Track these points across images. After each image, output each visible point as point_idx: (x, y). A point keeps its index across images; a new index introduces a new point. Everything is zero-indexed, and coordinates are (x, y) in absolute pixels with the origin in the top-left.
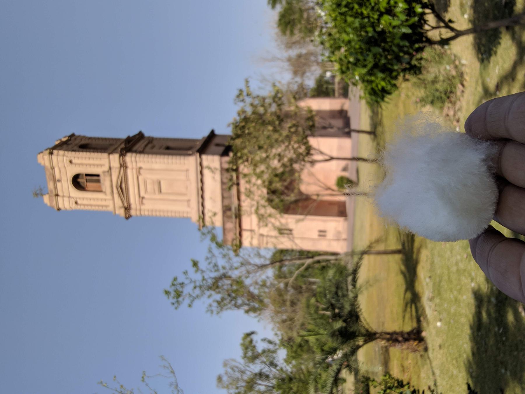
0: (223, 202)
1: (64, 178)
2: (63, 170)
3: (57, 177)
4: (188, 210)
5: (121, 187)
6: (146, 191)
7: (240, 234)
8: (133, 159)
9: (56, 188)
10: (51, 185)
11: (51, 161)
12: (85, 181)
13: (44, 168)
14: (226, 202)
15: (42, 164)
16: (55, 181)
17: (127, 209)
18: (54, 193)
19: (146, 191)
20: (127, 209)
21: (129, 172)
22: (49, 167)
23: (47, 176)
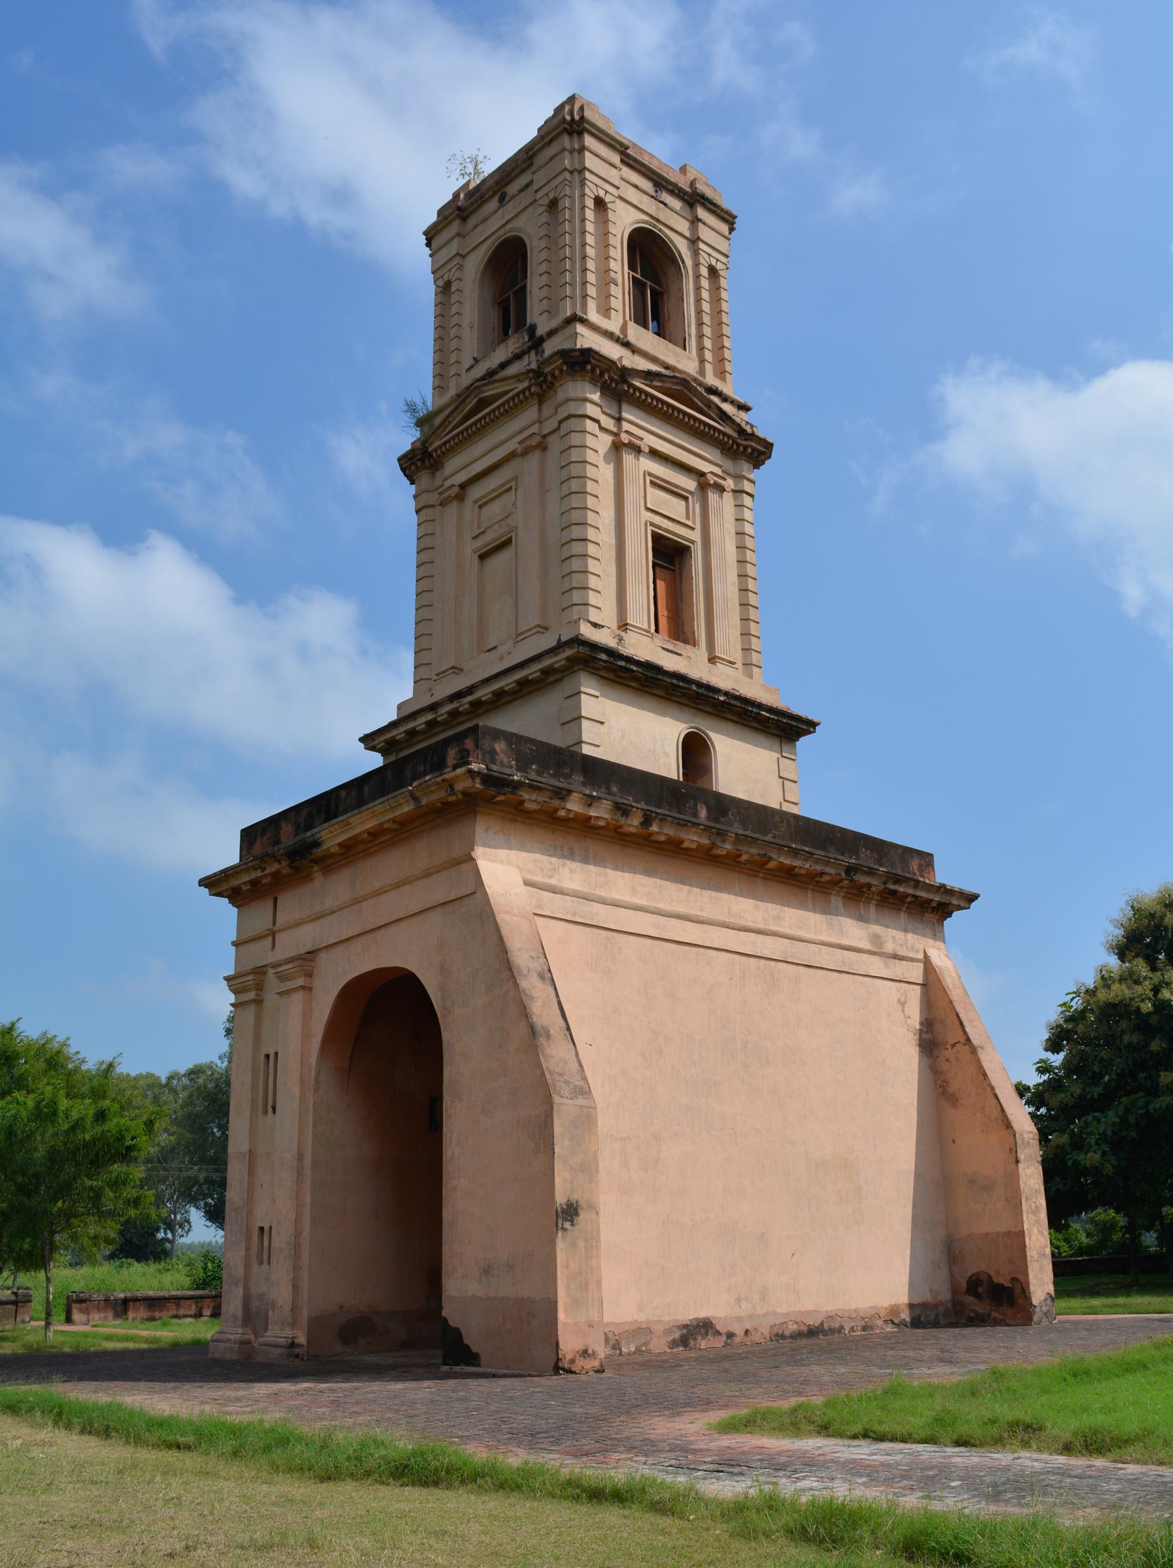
21: (530, 414)
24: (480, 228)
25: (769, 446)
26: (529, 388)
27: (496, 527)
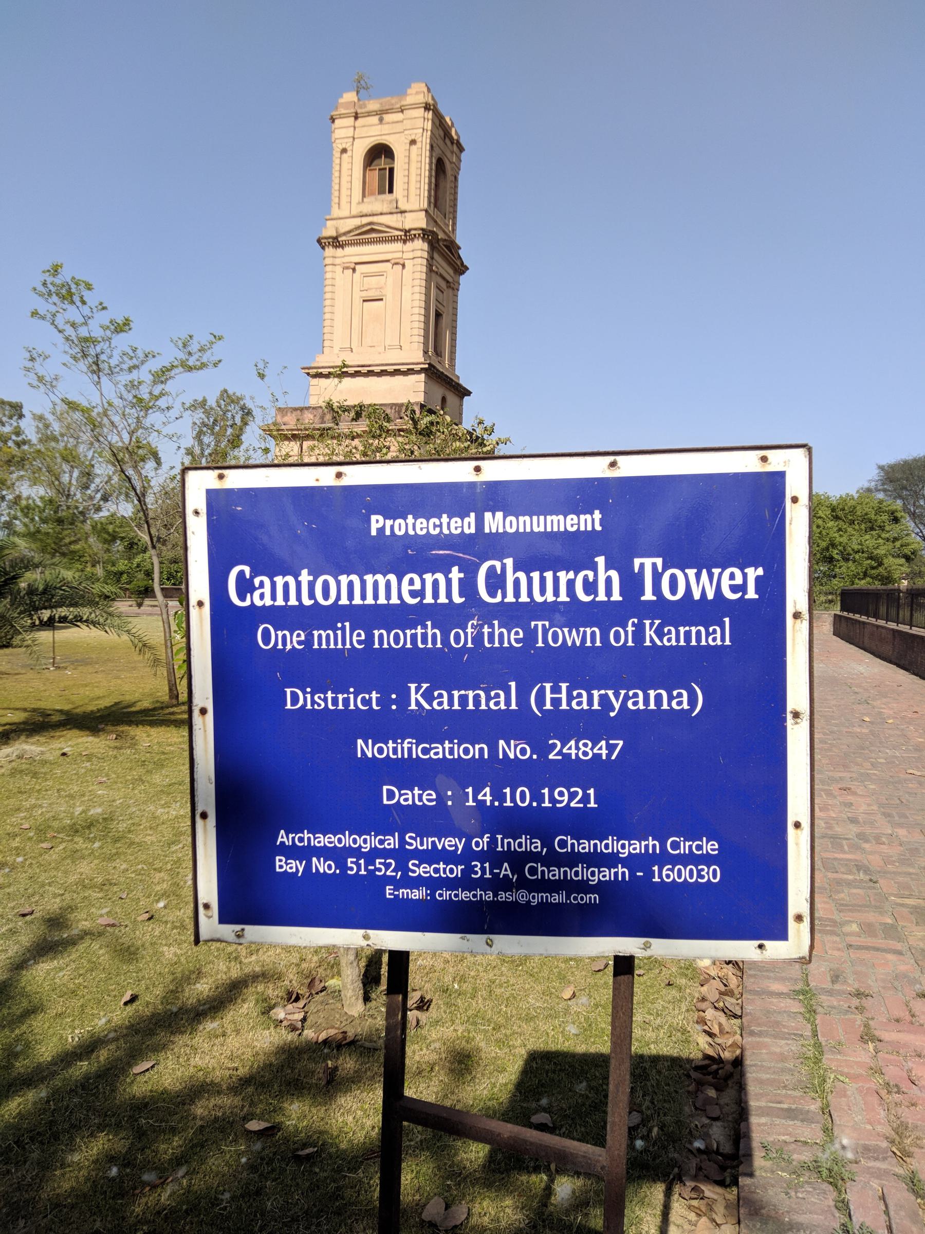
1: (386, 129)
2: (399, 127)
3: (388, 118)
4: (336, 350)
5: (372, 230)
6: (366, 276)
7: (295, 437)
8: (419, 253)
9: (369, 114)
10: (373, 105)
11: (414, 107)
12: (383, 166)
13: (404, 94)
15: (409, 91)
16: (381, 114)
17: (336, 242)
18: (359, 111)
19: (366, 276)
21: (398, 246)
22: (404, 103)
24: (365, 129)
25: (467, 269)
27: (374, 290)
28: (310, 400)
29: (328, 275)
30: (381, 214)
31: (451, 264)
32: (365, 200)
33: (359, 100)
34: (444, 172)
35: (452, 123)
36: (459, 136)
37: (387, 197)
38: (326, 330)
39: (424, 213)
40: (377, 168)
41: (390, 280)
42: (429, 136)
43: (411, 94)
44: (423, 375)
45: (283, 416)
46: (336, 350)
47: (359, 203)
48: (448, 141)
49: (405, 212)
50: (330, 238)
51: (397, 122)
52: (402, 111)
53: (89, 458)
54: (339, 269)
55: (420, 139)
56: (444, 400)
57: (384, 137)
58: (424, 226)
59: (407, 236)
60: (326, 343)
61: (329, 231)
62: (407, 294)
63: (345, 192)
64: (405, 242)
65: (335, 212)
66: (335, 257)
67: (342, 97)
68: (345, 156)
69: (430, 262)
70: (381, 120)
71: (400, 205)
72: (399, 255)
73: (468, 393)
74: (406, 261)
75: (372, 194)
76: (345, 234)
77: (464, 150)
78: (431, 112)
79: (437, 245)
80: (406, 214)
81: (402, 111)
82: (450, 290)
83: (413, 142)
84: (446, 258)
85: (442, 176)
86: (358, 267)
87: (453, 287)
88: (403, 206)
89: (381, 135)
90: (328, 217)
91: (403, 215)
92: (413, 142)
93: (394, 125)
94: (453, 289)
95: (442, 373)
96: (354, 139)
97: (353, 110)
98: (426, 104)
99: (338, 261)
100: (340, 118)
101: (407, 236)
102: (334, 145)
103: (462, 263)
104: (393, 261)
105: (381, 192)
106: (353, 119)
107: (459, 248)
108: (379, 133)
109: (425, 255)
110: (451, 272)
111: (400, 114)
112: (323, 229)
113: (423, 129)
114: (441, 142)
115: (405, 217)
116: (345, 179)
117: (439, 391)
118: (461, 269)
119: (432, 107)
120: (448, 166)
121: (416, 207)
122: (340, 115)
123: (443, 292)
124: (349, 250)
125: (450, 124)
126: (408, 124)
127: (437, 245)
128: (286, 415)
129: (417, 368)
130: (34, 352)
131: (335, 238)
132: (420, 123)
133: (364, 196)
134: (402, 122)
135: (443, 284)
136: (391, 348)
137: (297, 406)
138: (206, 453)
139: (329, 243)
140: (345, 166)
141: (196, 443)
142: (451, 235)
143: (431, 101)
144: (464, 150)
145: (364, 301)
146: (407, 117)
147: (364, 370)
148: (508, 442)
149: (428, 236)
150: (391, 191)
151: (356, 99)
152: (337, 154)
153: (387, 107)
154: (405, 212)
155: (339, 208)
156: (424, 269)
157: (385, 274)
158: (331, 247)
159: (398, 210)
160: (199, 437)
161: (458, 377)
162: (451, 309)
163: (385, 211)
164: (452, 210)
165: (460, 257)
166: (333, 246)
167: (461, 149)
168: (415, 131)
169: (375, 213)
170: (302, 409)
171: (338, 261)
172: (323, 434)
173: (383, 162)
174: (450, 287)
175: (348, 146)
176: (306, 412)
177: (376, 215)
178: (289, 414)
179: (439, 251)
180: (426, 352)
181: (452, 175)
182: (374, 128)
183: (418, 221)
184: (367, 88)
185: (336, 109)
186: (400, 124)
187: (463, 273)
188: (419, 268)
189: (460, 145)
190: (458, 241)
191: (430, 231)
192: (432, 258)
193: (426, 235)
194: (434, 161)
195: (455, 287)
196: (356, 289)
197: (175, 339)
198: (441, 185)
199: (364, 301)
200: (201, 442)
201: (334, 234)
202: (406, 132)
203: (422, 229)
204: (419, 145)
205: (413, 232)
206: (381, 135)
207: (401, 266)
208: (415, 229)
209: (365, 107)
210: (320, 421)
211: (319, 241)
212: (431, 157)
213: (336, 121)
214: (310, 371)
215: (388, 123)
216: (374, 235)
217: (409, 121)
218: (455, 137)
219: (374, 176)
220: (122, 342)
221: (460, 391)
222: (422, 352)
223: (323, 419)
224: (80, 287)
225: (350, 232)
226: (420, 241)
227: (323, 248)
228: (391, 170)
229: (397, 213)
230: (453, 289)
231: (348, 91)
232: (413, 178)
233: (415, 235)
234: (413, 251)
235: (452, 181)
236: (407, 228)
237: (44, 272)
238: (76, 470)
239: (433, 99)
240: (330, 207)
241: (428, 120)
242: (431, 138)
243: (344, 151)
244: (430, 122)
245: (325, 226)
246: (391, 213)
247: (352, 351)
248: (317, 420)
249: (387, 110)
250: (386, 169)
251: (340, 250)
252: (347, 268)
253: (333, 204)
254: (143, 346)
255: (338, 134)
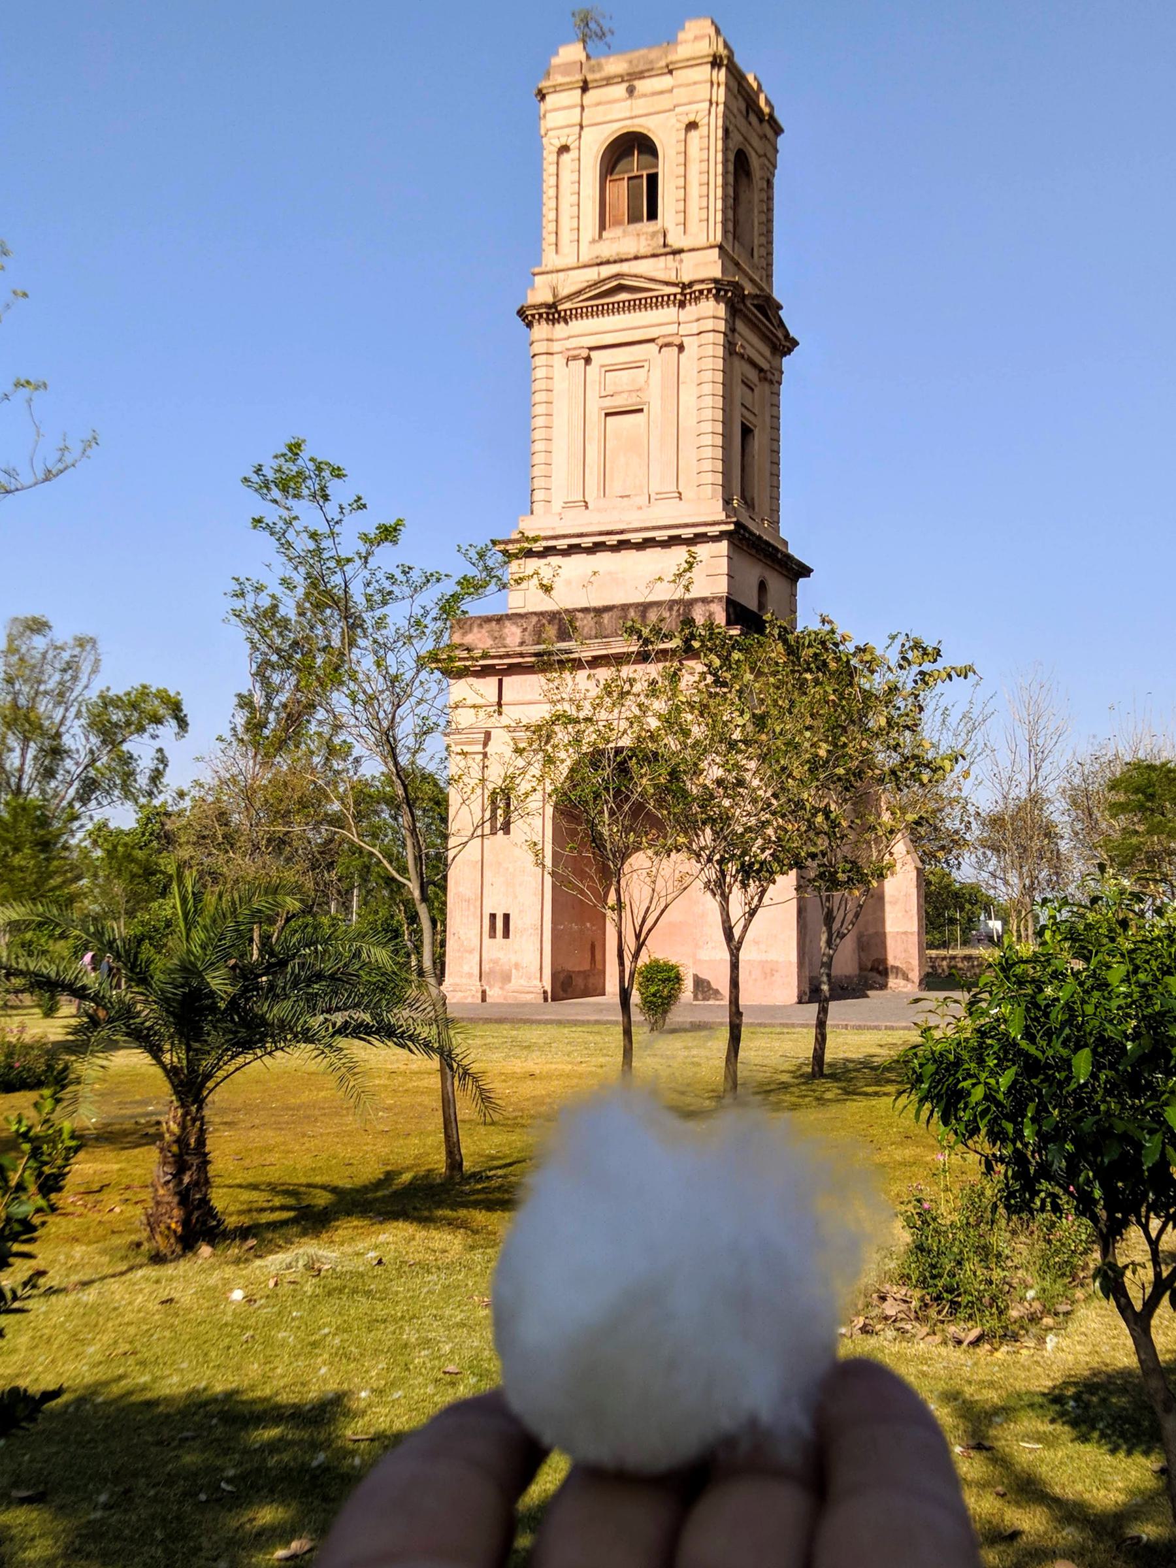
0: (585, 610)
1: (640, 105)
2: (665, 102)
3: (642, 86)
4: (557, 506)
5: (621, 288)
7: (486, 671)
8: (709, 324)
9: (609, 81)
10: (615, 65)
11: (691, 63)
12: (635, 173)
13: (672, 41)
14: (586, 623)
15: (681, 36)
16: (630, 79)
17: (553, 313)
18: (590, 77)
20: (553, 313)
22: (672, 57)
23: (643, 52)
25: (795, 343)
26: (675, 295)
27: (625, 395)
28: (510, 600)
29: (540, 373)
30: (636, 258)
31: (766, 338)
32: (605, 234)
33: (588, 57)
34: (749, 174)
35: (759, 85)
36: (772, 107)
37: (646, 226)
38: (537, 471)
39: (717, 250)
40: (626, 177)
41: (656, 375)
42: (720, 115)
43: (686, 42)
44: (724, 544)
45: (464, 634)
46: (557, 506)
47: (593, 241)
48: (753, 119)
49: (680, 251)
50: (541, 305)
51: (662, 92)
52: (670, 72)
53: (57, 721)
54: (559, 360)
55: (705, 121)
56: (762, 586)
57: (637, 121)
58: (717, 273)
59: (686, 294)
60: (539, 495)
61: (540, 294)
62: (688, 397)
63: (567, 223)
64: (682, 305)
65: (550, 259)
66: (548, 340)
67: (557, 54)
68: (565, 157)
69: (730, 338)
70: (631, 91)
71: (670, 241)
72: (673, 329)
73: (805, 571)
74: (684, 339)
75: (617, 223)
76: (569, 297)
77: (782, 131)
78: (723, 70)
79: (741, 306)
80: (683, 255)
81: (670, 72)
82: (766, 386)
83: (692, 126)
84: (754, 325)
85: (744, 180)
86: (593, 354)
87: (770, 378)
88: (675, 241)
89: (632, 118)
90: (537, 270)
91: (678, 257)
92: (692, 126)
93: (655, 97)
94: (771, 382)
95: (760, 538)
96: (581, 127)
97: (579, 77)
98: (715, 56)
99: (556, 347)
100: (555, 91)
101: (686, 294)
102: (545, 140)
103: (787, 335)
104: (660, 342)
105: (634, 218)
106: (579, 91)
107: (780, 307)
108: (628, 114)
109: (721, 326)
110: (767, 352)
111: (668, 77)
112: (529, 292)
113: (711, 103)
114: (741, 122)
115: (681, 261)
116: (567, 199)
117: (753, 573)
118: (783, 345)
119: (725, 62)
120: (755, 162)
121: (702, 241)
122: (554, 86)
123: (752, 390)
124: (577, 326)
125: (755, 86)
126: (681, 95)
127: (741, 306)
128: (471, 630)
129: (714, 530)
130: (247, 584)
131: (553, 306)
132: (704, 91)
133: (602, 227)
134: (671, 91)
135: (753, 375)
136: (662, 496)
137: (490, 613)
138: (276, 703)
139: (541, 315)
140: (567, 177)
141: (258, 685)
142: (764, 285)
143: (722, 51)
144: (782, 131)
145: (607, 415)
146: (680, 82)
147: (612, 540)
148: (970, 674)
149: (726, 292)
150: (653, 215)
151: (583, 57)
152: (550, 156)
153: (641, 67)
154: (680, 251)
155: (557, 252)
156: (720, 351)
157: (646, 364)
158: (543, 322)
159: (668, 250)
160: (261, 674)
161: (786, 543)
162: (768, 419)
163: (643, 251)
164: (763, 240)
165: (781, 324)
166: (547, 320)
167: (778, 130)
168: (695, 107)
169: (624, 257)
170: (499, 619)
171: (556, 347)
172: (544, 663)
173: (635, 164)
174: (766, 379)
175: (571, 141)
176: (507, 623)
177: (627, 260)
178: (475, 630)
179: (746, 316)
180: (727, 502)
181: (762, 178)
182: (617, 105)
183: (708, 266)
184: (602, 36)
185: (547, 75)
186: (667, 95)
187: (789, 351)
188: (710, 350)
189: (775, 122)
190: (777, 295)
191: (730, 283)
192: (733, 330)
193: (721, 290)
194: (732, 157)
195: (775, 378)
196: (592, 395)
197: (464, 547)
198: (743, 197)
199: (607, 415)
200: (266, 682)
201: (550, 300)
202: (678, 110)
203: (715, 281)
204: (703, 130)
205: (697, 287)
206: (632, 118)
207: (676, 349)
208: (702, 281)
209: (600, 67)
210: (535, 638)
211: (521, 313)
212: (725, 150)
213: (548, 98)
214: (510, 547)
215: (644, 96)
216: (624, 296)
217: (682, 90)
218: (766, 110)
219: (619, 191)
220: (386, 558)
221: (790, 569)
222: (721, 501)
223: (540, 636)
224: (323, 474)
225: (579, 292)
226: (712, 302)
227: (529, 325)
228: (653, 180)
229: (666, 254)
230: (771, 382)
231: (566, 42)
232: (695, 190)
233: (701, 292)
234: (698, 320)
235: (761, 190)
236: (686, 280)
237: (276, 457)
238: (32, 744)
239: (726, 46)
240: (540, 251)
241: (719, 85)
242: (725, 116)
243: (564, 149)
244: (722, 89)
245: (532, 286)
246: (654, 256)
247: (587, 507)
248: (529, 638)
249: (642, 72)
250: (642, 176)
251: (560, 328)
252: (575, 358)
253: (545, 246)
254: (422, 564)
255: (553, 120)
